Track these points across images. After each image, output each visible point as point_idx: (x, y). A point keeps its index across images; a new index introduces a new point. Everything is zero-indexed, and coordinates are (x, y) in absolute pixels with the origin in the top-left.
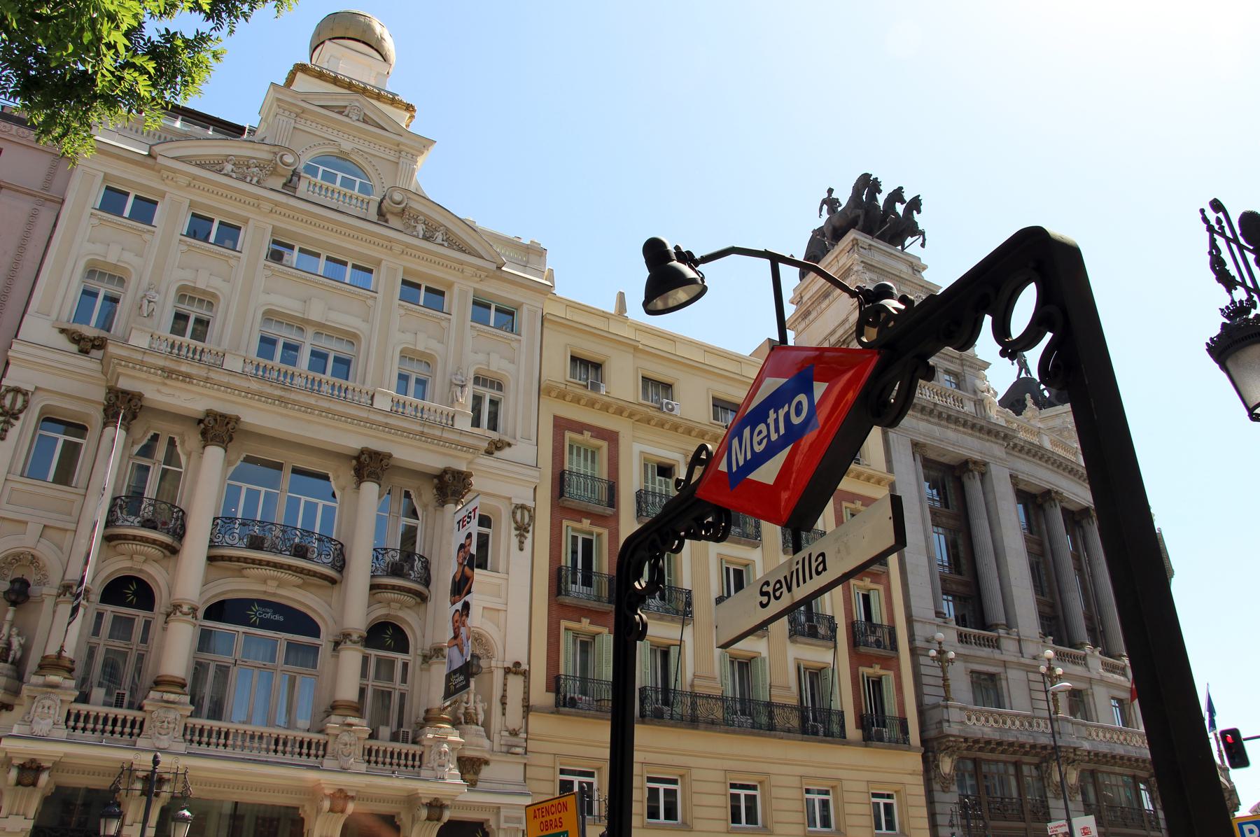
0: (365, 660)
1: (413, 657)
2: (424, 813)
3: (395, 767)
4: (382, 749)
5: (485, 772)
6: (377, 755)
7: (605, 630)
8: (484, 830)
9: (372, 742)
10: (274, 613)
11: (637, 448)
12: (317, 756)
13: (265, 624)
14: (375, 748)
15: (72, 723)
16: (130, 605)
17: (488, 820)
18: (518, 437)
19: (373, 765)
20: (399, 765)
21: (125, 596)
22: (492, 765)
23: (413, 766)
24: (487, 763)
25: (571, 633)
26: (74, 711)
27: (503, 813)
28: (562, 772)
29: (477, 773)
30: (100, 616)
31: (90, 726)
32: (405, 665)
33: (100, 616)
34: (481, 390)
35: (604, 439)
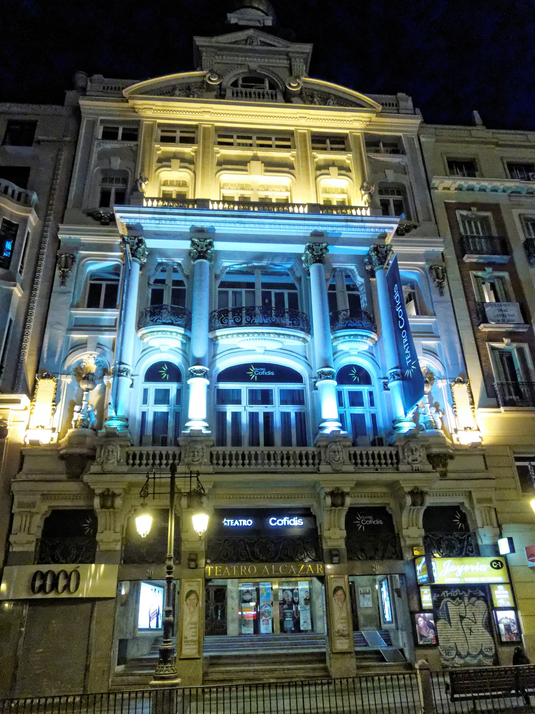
0: (339, 394)
1: (376, 385)
2: (409, 500)
3: (378, 466)
4: (364, 453)
5: (452, 465)
6: (361, 458)
7: (385, 651)
8: (461, 512)
9: (355, 449)
10: (267, 371)
11: (516, 212)
12: (313, 464)
13: (262, 379)
14: (358, 453)
15: (131, 462)
16: (165, 380)
17: (463, 504)
18: (421, 218)
19: (360, 466)
20: (380, 464)
21: (160, 375)
22: (456, 458)
23: (392, 464)
24: (451, 457)
25: (497, 353)
26: (131, 453)
27: (475, 496)
28: (518, 459)
29: (445, 465)
30: (146, 391)
31: (144, 462)
32: (371, 394)
33: (146, 391)
34: (385, 197)
35: (486, 210)
